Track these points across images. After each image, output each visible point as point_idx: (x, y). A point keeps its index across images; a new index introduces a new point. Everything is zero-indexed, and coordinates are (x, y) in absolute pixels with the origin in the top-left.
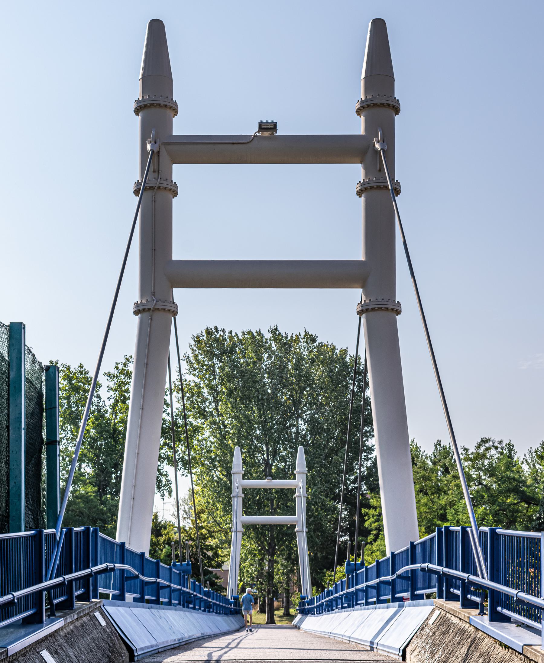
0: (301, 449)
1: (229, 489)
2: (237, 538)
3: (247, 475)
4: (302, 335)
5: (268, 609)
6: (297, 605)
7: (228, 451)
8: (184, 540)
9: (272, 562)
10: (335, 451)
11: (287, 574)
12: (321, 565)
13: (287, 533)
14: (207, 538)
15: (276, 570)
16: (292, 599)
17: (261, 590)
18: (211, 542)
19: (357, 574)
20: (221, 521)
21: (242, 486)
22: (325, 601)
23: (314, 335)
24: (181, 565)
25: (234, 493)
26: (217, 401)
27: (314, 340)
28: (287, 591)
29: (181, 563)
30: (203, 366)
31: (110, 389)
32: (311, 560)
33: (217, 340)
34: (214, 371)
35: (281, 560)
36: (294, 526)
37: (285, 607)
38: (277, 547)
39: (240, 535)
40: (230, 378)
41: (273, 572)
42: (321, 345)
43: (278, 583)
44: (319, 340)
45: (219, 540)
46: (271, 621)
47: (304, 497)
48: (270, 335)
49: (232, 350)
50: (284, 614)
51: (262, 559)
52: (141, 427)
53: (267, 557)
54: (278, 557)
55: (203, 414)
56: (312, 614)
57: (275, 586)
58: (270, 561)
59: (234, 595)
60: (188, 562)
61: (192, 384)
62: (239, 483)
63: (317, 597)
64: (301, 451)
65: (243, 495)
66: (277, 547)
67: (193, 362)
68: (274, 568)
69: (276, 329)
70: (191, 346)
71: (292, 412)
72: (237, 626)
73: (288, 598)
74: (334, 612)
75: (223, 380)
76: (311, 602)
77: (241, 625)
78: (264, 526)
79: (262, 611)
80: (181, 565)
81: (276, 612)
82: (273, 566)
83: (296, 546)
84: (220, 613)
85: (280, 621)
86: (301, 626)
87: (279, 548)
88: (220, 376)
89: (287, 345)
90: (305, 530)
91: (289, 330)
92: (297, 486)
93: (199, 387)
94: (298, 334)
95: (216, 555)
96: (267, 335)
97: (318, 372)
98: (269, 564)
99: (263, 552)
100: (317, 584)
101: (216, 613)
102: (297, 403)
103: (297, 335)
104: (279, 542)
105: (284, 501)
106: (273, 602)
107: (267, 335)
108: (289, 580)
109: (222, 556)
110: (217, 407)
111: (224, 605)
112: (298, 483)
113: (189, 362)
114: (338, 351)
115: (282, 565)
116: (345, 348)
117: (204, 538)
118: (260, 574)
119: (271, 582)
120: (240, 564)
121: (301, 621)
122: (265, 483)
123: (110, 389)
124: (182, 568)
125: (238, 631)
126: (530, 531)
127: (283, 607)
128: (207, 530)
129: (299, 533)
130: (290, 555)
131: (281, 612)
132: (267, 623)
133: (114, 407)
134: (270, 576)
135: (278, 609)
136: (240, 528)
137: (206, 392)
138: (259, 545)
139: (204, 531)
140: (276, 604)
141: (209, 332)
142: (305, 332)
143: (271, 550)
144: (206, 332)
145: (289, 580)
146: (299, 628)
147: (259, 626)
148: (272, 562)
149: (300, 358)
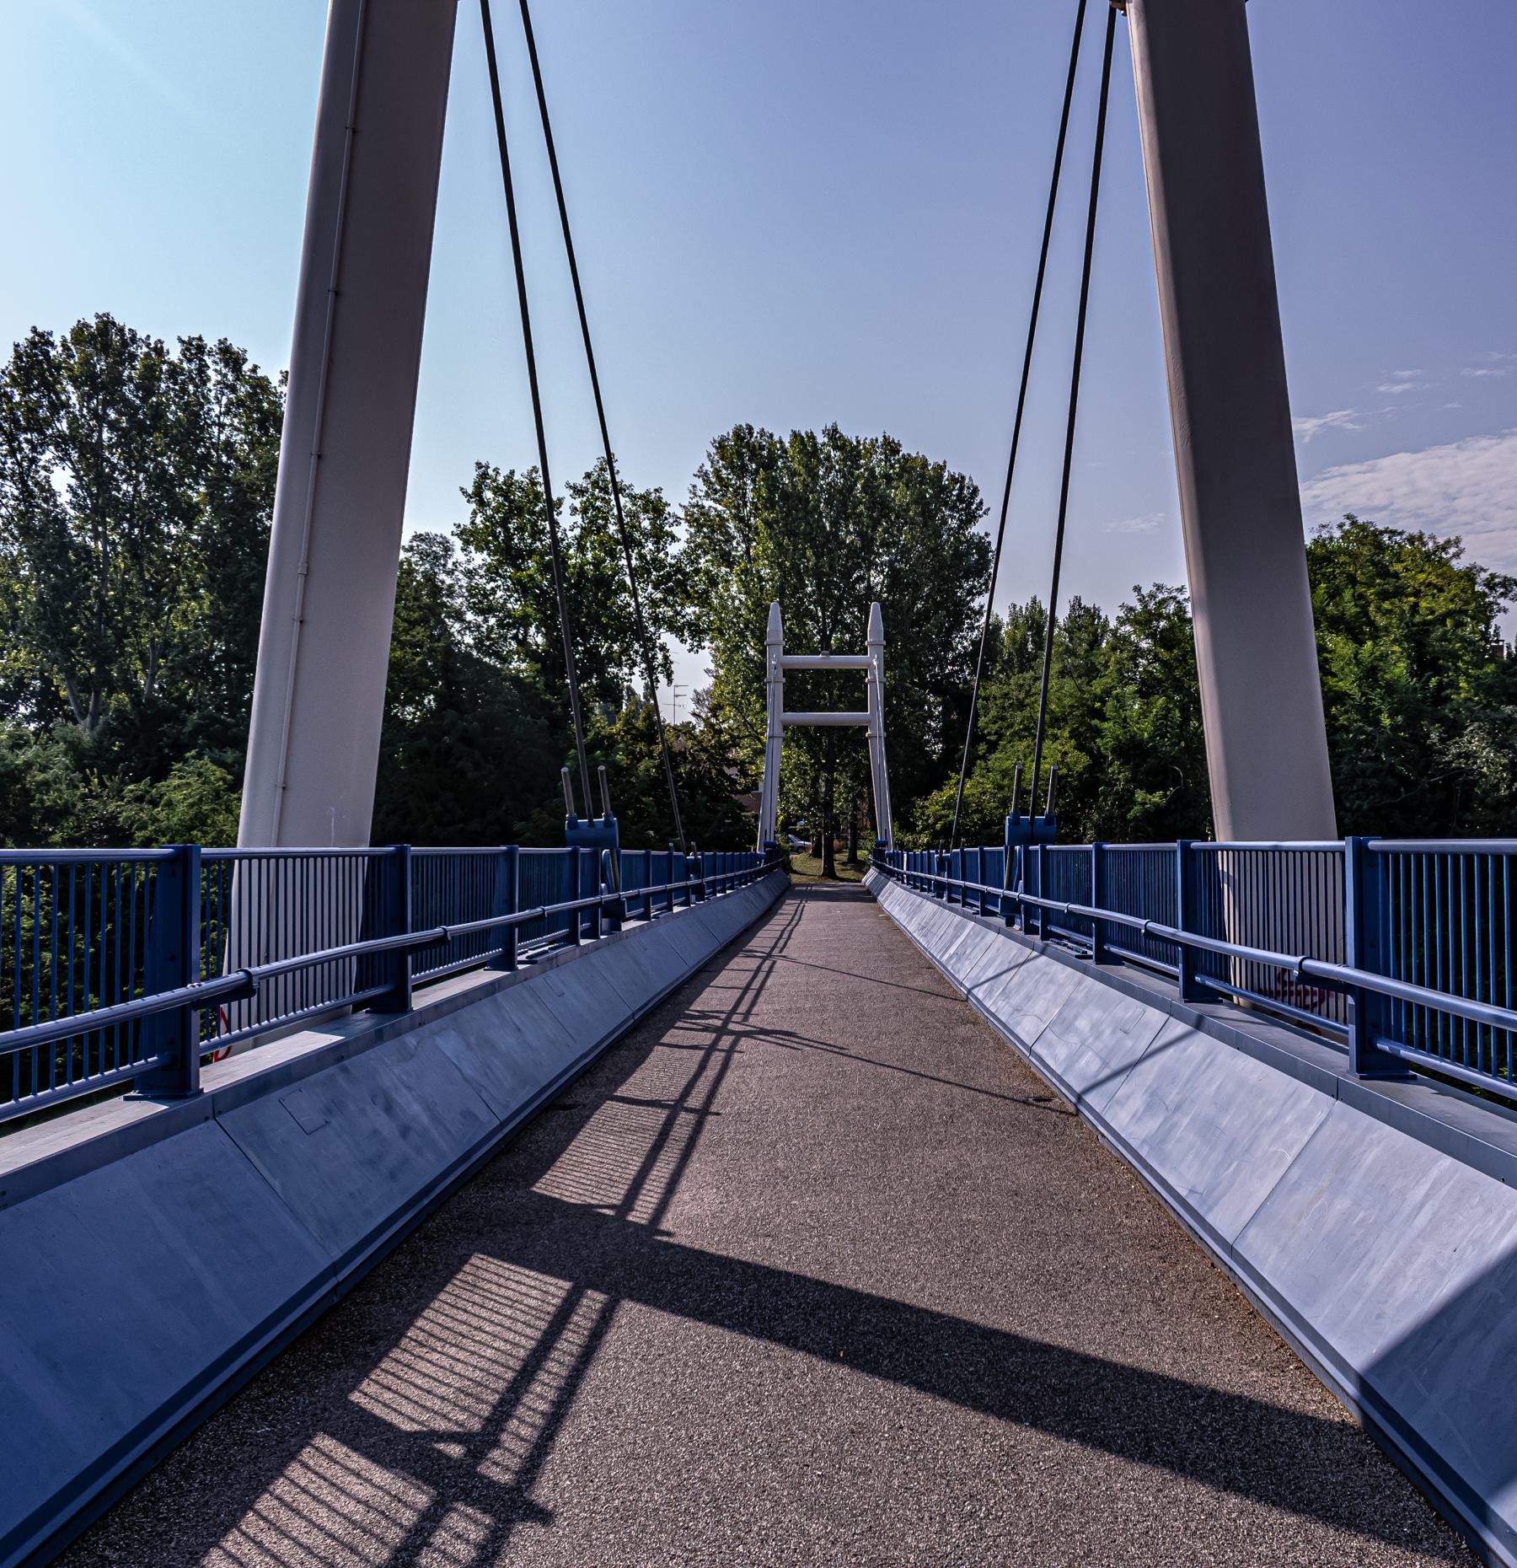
0: (874, 606)
1: (762, 666)
2: (779, 751)
7: (761, 609)
9: (830, 783)
10: (924, 616)
11: (854, 801)
12: (916, 777)
13: (856, 737)
24: (591, 824)
26: (747, 540)
27: (895, 451)
28: (854, 826)
29: (591, 821)
31: (574, 510)
32: (892, 780)
34: (744, 495)
35: (844, 779)
36: (866, 729)
40: (770, 504)
41: (832, 797)
44: (904, 451)
49: (772, 459)
51: (815, 780)
52: (330, 360)
55: (726, 559)
57: (835, 818)
58: (827, 781)
62: (776, 659)
69: (835, 430)
70: (709, 455)
71: (863, 554)
72: (769, 899)
75: (757, 509)
78: (819, 728)
79: (816, 854)
80: (591, 824)
81: (837, 856)
88: (753, 503)
89: (852, 453)
90: (883, 734)
92: (870, 664)
93: (723, 520)
97: (898, 495)
99: (818, 767)
100: (904, 820)
102: (867, 542)
105: (850, 688)
107: (821, 439)
108: (856, 808)
110: (748, 549)
112: (872, 660)
113: (707, 481)
117: (723, 747)
120: (782, 786)
122: (817, 660)
126: (1199, 737)
131: (843, 856)
134: (828, 805)
135: (840, 851)
136: (779, 731)
140: (836, 842)
141: (739, 434)
145: (856, 808)
146: (874, 900)
148: (830, 783)
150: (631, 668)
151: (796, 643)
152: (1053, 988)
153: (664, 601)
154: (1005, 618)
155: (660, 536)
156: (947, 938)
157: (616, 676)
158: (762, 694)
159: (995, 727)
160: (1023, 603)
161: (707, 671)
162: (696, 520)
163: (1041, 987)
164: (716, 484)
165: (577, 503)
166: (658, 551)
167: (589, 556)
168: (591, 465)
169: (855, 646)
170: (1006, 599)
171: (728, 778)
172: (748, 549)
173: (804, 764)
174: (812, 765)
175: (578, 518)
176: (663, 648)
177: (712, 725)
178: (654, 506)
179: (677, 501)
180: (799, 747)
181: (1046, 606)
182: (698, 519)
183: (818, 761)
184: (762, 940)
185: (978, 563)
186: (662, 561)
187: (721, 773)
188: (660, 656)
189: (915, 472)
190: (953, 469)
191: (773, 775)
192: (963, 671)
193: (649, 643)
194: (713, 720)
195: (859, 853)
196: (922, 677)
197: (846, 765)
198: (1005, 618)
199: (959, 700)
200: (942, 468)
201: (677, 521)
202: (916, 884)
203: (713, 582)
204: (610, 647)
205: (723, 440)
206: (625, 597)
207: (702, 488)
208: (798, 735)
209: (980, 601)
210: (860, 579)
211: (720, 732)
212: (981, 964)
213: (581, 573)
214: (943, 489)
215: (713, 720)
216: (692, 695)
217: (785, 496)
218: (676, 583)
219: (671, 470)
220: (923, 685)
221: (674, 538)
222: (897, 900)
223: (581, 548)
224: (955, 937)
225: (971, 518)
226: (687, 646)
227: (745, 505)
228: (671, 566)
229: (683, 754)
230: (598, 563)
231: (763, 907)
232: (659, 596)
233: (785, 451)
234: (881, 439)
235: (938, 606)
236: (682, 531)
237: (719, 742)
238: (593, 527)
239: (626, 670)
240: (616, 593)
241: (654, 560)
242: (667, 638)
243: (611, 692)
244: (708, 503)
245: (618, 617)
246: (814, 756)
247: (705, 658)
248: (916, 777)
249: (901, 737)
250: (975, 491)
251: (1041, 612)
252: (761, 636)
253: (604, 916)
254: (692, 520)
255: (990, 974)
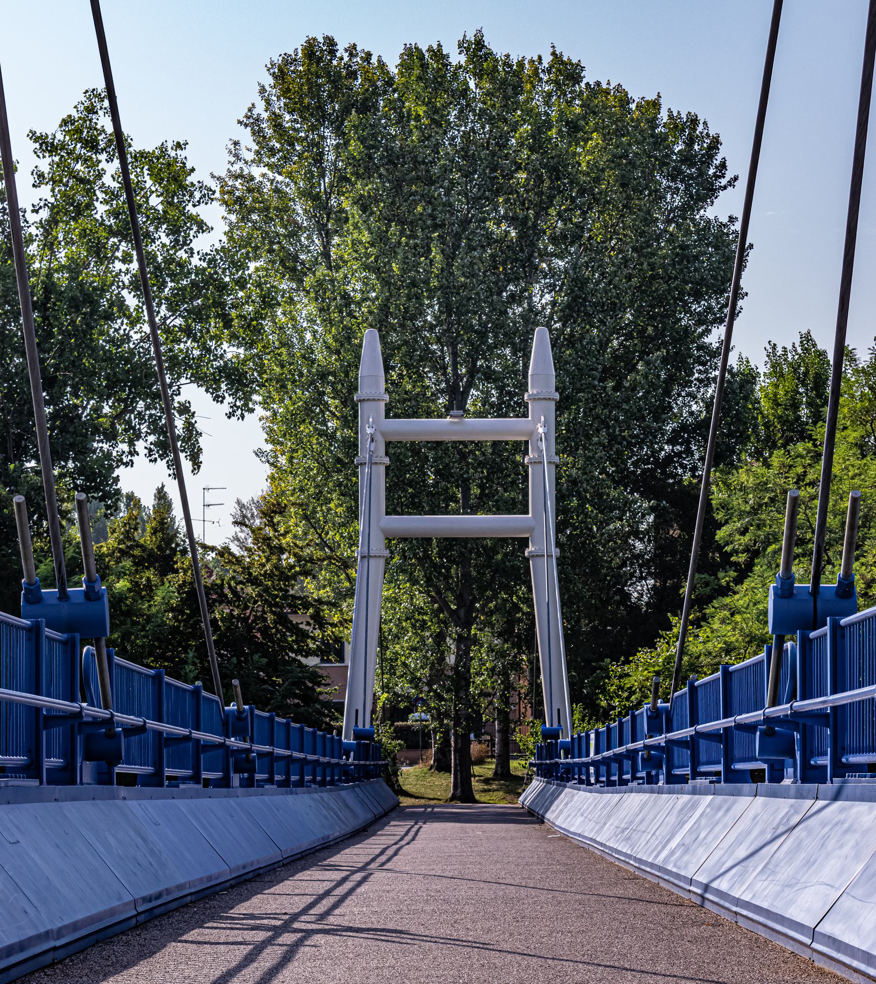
1: (351, 446)
3: (390, 412)
4: (546, 64)
5: (456, 762)
6: (532, 754)
7: (347, 341)
8: (233, 583)
9: (466, 642)
10: (626, 360)
12: (605, 632)
13: (504, 564)
14: (294, 577)
15: (475, 663)
16: (517, 737)
17: (439, 716)
18: (310, 587)
19: (838, 631)
20: (337, 538)
21: (383, 434)
22: (646, 747)
23: (574, 61)
25: (363, 455)
28: (504, 717)
29: (63, 590)
30: (292, 145)
31: (40, 178)
33: (335, 79)
36: (524, 543)
37: (499, 756)
38: (477, 605)
39: (377, 567)
40: (365, 168)
42: (596, 90)
43: (480, 695)
44: (589, 77)
45: (333, 590)
46: (464, 793)
47: (549, 463)
48: (463, 59)
49: (366, 106)
50: (496, 774)
51: (439, 638)
53: (454, 630)
54: (481, 630)
55: (292, 267)
56: (581, 782)
57: (471, 702)
58: (460, 639)
59: (360, 727)
60: (90, 581)
61: (267, 188)
62: (375, 426)
63: (597, 734)
64: (541, 340)
65: (387, 461)
66: (477, 605)
67: (269, 132)
68: (472, 659)
69: (479, 43)
70: (263, 90)
71: (521, 261)
72: (364, 816)
73: (506, 732)
74: (687, 787)
76: (578, 746)
77: (379, 810)
79: (442, 766)
81: (476, 770)
82: (467, 653)
83: (529, 602)
84: (300, 783)
85: (485, 791)
86: (549, 816)
87: (483, 606)
89: (509, 82)
90: (555, 552)
91: (510, 44)
92: (532, 433)
94: (536, 58)
95: (319, 621)
96: (457, 58)
97: (586, 155)
98: (458, 647)
100: (586, 695)
101: (281, 784)
102: (529, 233)
103: (532, 61)
104: (482, 589)
105: (497, 475)
106: (469, 742)
107: (457, 58)
109: (334, 625)
111: (326, 759)
112: (536, 427)
113: (258, 133)
114: (633, 106)
115: (491, 649)
116: (651, 97)
118: (437, 675)
119: (462, 694)
121: (546, 800)
123: (40, 178)
124: (65, 610)
125: (360, 833)
127: (493, 757)
128: (295, 555)
129: (538, 560)
130: (511, 622)
131: (488, 769)
132: (453, 798)
133: (48, 227)
135: (480, 762)
136: (378, 546)
137: (300, 209)
138: (434, 601)
139: (288, 560)
140: (475, 748)
141: (310, 49)
142: (554, 54)
143: (462, 613)
144: (305, 55)
145: (508, 686)
146: (541, 820)
147: (429, 815)
148: (466, 642)
149: (542, 126)
150: (131, 443)
151: (404, 405)
152: (851, 840)
153: (188, 331)
154: (760, 364)
155: (181, 225)
156: (664, 831)
157: (108, 456)
158: (350, 493)
159: (746, 539)
160: (788, 340)
161: (259, 453)
162: (240, 200)
163: (831, 844)
164: (272, 138)
165: (45, 164)
166: (176, 244)
167: (62, 255)
168: (69, 104)
169: (511, 404)
170: (768, 323)
171: (295, 629)
172: (326, 245)
173: (420, 611)
174: (436, 613)
175: (45, 192)
176: (185, 409)
177: (267, 539)
178: (171, 172)
179: (207, 163)
180: (414, 582)
181: (826, 343)
182: (241, 199)
183: (444, 606)
184: (353, 855)
185: (716, 268)
186: (181, 265)
187: (282, 619)
188: (179, 423)
189: (608, 110)
190: (676, 104)
191: (371, 638)
192: (689, 452)
193: (163, 398)
194: (269, 531)
195: (513, 764)
196: (618, 460)
197: (492, 613)
198: (760, 364)
199: (681, 505)
200: (656, 105)
201: (208, 196)
202: (614, 774)
203: (268, 302)
204: (97, 410)
205: (288, 60)
206: (120, 325)
207: (246, 137)
208: (413, 557)
209: (715, 337)
210: (514, 299)
211: (281, 550)
212: (725, 845)
213: (49, 288)
214: (659, 141)
215: (269, 531)
216: (232, 508)
217: (392, 159)
218: (206, 297)
219: (200, 111)
220: (623, 479)
221: (202, 227)
222: (579, 811)
223: (50, 245)
224: (681, 824)
225: (708, 191)
226: (225, 408)
227: (322, 175)
228: (199, 271)
229: (218, 588)
230: (74, 268)
231: (352, 824)
232: (179, 321)
233: (390, 82)
234: (547, 60)
235: (648, 343)
236: (214, 214)
237: (277, 567)
238: (71, 207)
239: (125, 447)
240: (109, 317)
241: (169, 260)
242: (191, 393)
243: (98, 480)
244: (257, 172)
245: (108, 358)
246: (438, 598)
247: (253, 429)
248: (605, 632)
249: (579, 559)
250: (715, 143)
251: (822, 354)
252: (348, 394)
253: (87, 757)
254: (234, 202)
255: (742, 853)
